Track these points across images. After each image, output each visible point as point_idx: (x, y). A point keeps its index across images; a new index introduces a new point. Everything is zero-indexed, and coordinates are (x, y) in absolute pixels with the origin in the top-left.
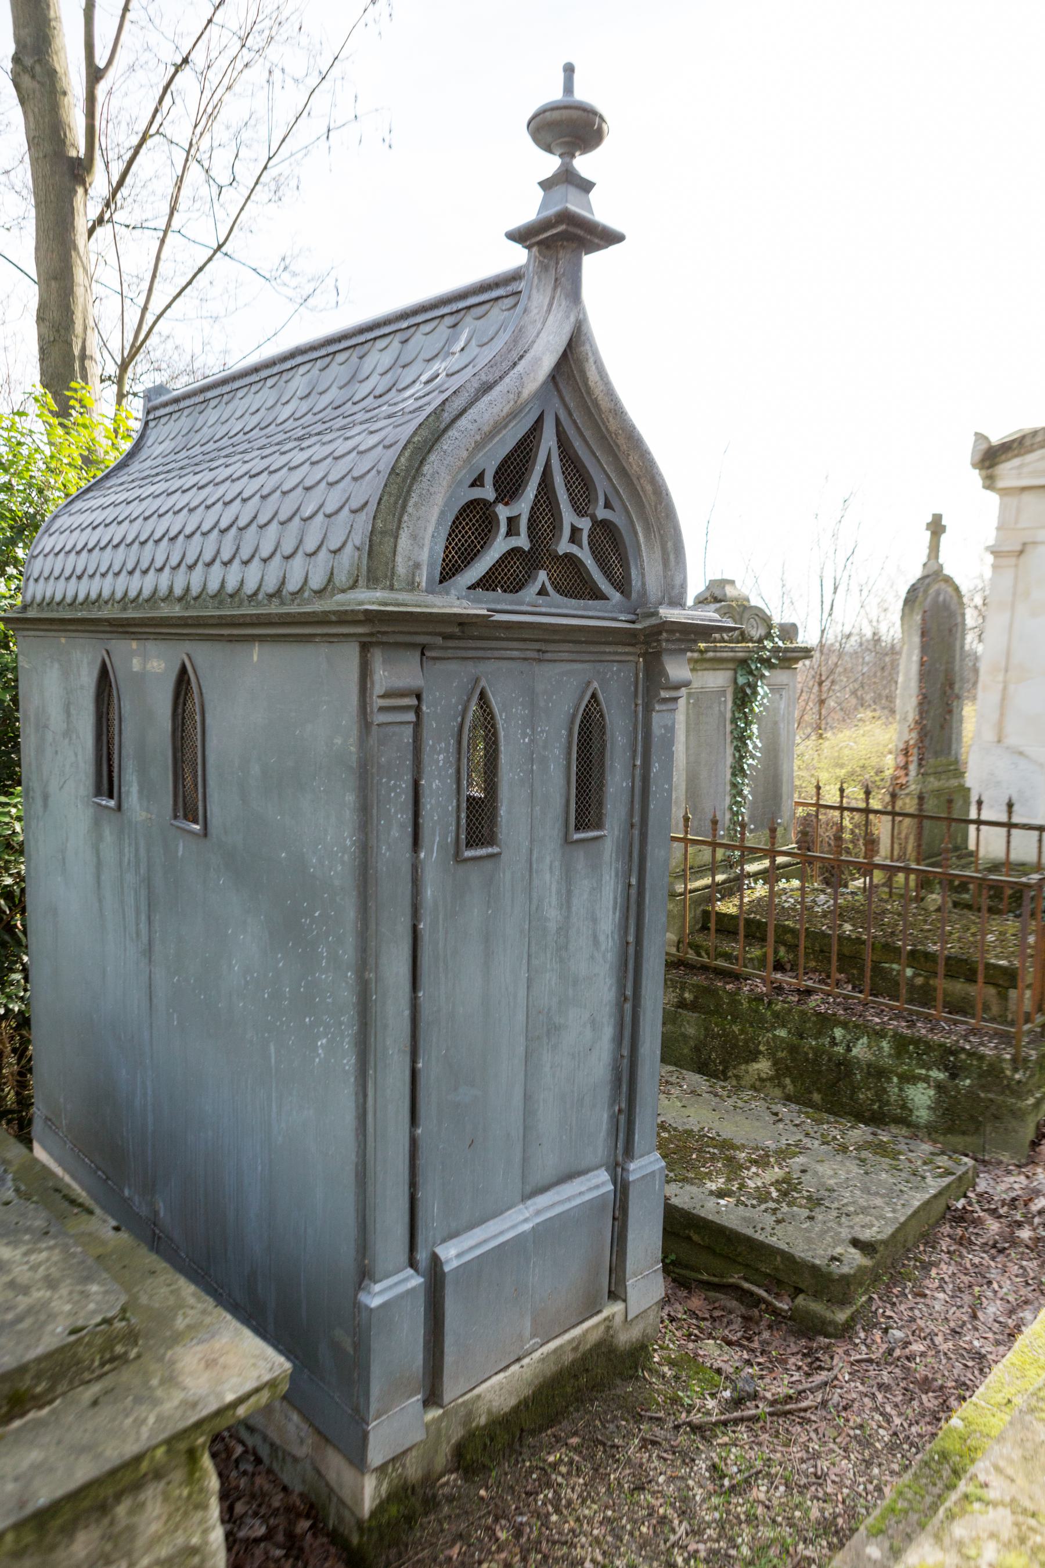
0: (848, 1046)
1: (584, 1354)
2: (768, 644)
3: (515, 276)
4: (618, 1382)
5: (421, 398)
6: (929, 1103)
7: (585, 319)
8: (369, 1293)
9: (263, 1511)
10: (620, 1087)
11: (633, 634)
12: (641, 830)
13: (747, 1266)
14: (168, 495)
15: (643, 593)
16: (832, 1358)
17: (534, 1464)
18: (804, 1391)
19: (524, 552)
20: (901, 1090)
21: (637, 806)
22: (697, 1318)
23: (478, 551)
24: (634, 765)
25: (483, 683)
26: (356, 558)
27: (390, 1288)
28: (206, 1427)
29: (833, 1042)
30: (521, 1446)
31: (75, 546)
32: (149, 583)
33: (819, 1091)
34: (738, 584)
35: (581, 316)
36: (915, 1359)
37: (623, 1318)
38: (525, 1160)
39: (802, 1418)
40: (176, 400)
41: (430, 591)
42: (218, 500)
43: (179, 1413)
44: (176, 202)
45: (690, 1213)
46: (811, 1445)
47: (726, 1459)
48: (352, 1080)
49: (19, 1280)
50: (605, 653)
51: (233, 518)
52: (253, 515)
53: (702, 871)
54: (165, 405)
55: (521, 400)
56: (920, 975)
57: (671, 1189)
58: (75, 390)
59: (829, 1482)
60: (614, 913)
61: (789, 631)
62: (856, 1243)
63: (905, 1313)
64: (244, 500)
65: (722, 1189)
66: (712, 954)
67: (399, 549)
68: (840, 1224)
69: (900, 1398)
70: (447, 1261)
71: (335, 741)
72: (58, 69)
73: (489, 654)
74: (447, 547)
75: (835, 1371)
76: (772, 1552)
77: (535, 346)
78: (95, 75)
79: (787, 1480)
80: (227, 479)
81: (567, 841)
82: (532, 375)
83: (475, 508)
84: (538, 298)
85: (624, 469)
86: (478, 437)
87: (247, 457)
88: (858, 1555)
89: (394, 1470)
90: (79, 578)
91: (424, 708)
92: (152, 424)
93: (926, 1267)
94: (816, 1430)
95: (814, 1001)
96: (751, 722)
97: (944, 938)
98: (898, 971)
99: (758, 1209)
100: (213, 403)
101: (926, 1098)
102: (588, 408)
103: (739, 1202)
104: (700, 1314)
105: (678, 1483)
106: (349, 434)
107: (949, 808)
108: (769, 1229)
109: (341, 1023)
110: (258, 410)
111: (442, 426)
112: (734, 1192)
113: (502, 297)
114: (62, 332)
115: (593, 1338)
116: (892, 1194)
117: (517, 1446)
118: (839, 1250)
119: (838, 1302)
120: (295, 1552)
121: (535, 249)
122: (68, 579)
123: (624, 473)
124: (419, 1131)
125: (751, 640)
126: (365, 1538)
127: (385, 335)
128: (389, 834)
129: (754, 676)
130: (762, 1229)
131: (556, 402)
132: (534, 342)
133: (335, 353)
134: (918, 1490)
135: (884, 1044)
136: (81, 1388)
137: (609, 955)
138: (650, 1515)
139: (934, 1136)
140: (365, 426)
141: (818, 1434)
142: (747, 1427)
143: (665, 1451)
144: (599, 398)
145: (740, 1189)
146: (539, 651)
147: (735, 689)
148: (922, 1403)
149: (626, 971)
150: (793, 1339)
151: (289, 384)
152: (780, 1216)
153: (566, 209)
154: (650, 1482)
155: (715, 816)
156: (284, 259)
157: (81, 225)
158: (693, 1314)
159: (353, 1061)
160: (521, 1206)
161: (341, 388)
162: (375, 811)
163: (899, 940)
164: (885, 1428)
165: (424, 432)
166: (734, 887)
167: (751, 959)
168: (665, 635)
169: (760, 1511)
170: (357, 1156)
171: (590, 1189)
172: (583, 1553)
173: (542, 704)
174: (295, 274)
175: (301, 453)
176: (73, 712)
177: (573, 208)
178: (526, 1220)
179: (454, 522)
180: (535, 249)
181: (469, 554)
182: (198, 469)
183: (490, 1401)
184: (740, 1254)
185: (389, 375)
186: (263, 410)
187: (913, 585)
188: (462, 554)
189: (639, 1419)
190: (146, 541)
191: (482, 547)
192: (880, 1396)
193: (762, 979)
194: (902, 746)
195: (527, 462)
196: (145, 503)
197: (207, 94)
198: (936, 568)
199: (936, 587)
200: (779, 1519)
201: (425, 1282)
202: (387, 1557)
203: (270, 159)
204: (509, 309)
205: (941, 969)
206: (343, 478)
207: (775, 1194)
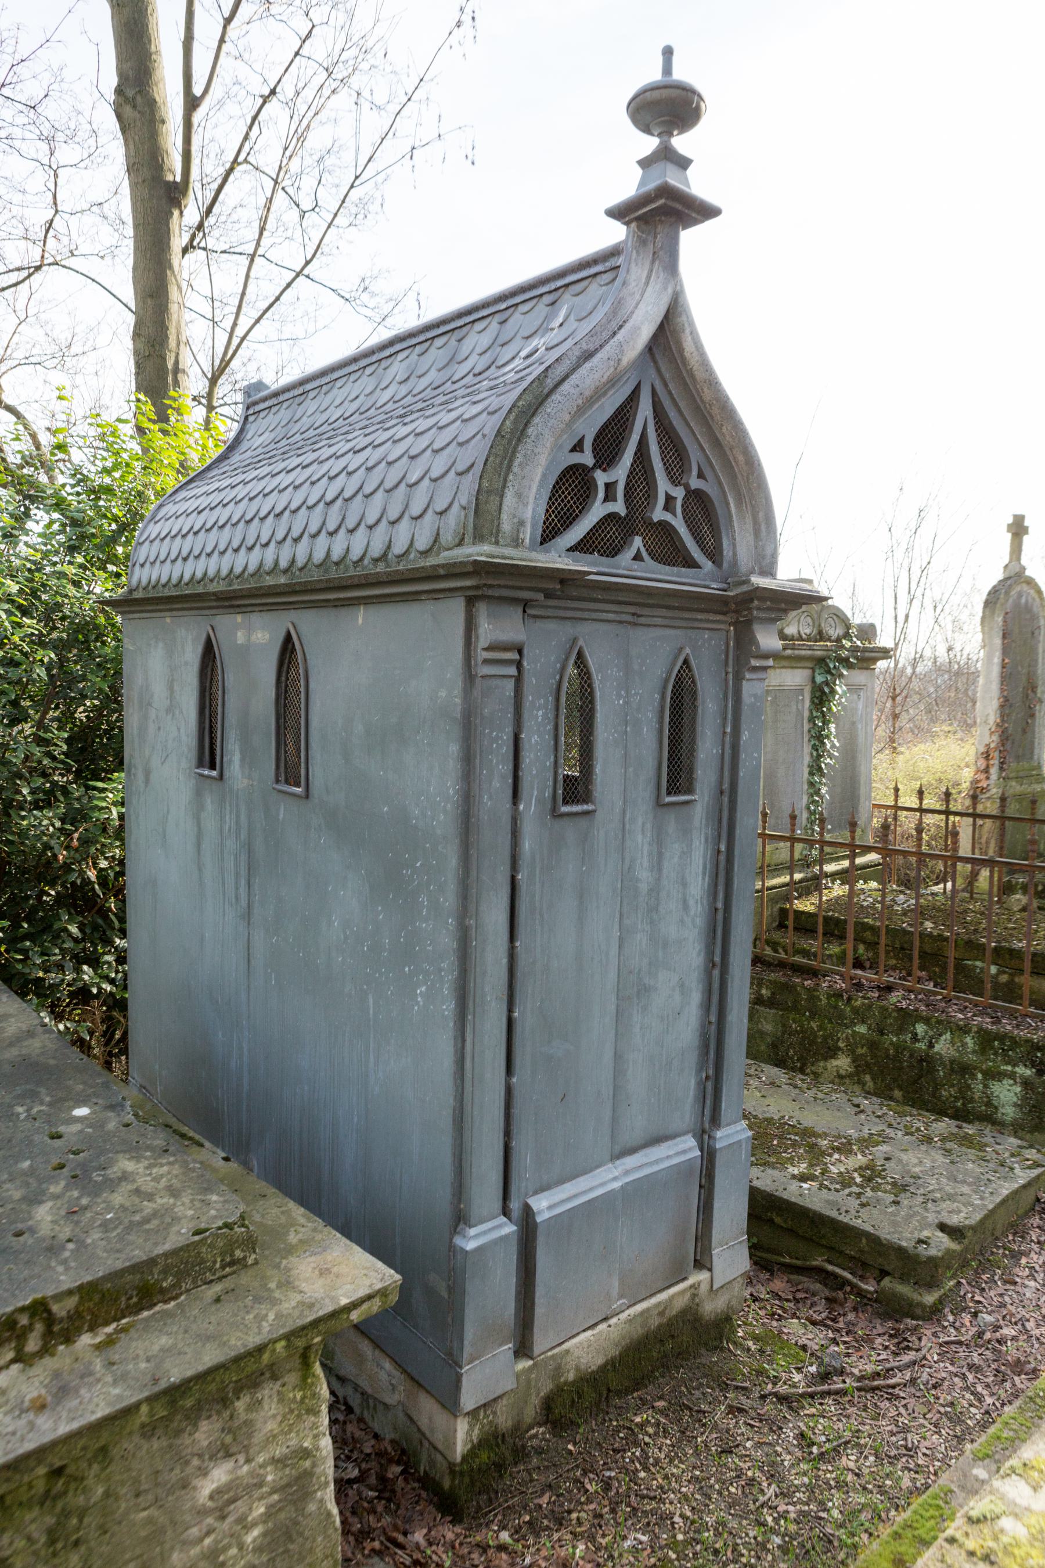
0: (930, 1042)
1: (670, 1320)
2: (847, 644)
3: (615, 252)
4: (703, 1351)
5: (521, 371)
6: (1015, 1099)
7: (682, 291)
8: (464, 1236)
9: (355, 1456)
10: (707, 1053)
11: (724, 601)
12: (730, 796)
13: (831, 1248)
14: (273, 476)
15: (735, 563)
16: (920, 1339)
17: (621, 1423)
18: (892, 1369)
19: (620, 518)
20: (986, 1086)
21: (726, 773)
22: (780, 1298)
23: (577, 516)
24: (724, 733)
25: (581, 642)
26: (462, 517)
27: (485, 1233)
28: (322, 1327)
29: (915, 1038)
30: (608, 1406)
31: (180, 530)
32: (254, 560)
33: (900, 1088)
34: (816, 583)
35: (678, 288)
36: (1006, 1342)
37: (708, 1287)
38: (615, 1119)
39: (890, 1394)
40: (276, 394)
41: (531, 548)
42: (323, 476)
43: (296, 1313)
44: (265, 223)
45: (772, 1195)
46: (900, 1420)
47: (813, 1429)
48: (452, 1024)
49: (143, 1189)
50: (697, 620)
51: (339, 490)
52: (358, 486)
53: (779, 869)
54: (264, 399)
55: (620, 368)
56: (1004, 972)
57: (755, 1172)
58: (175, 399)
59: (920, 1454)
60: (703, 879)
61: (868, 631)
62: (943, 1227)
63: (995, 1299)
64: (349, 474)
65: (804, 1174)
66: (790, 950)
67: (505, 507)
68: (926, 1210)
69: (992, 1378)
70: (539, 1212)
71: (440, 694)
72: (158, 99)
73: (586, 615)
74: (547, 511)
75: (924, 1351)
76: (863, 1517)
77: (634, 316)
78: (192, 103)
79: (877, 1451)
80: (331, 457)
81: (659, 804)
82: (631, 343)
83: (574, 473)
84: (636, 272)
85: (717, 439)
86: (580, 402)
87: (350, 436)
88: (965, 1476)
89: (486, 1416)
90: (185, 559)
91: (525, 664)
92: (251, 419)
93: (1016, 1256)
94: (905, 1406)
95: (894, 997)
96: (829, 721)
97: (1029, 936)
98: (982, 969)
99: (842, 1193)
100: (312, 394)
101: (1012, 1094)
102: (683, 378)
103: (821, 1186)
104: (783, 1295)
105: (766, 1449)
106: (451, 407)
107: (1033, 809)
108: (853, 1212)
109: (440, 970)
110: (357, 397)
111: (546, 391)
112: (817, 1177)
113: (601, 273)
114: (157, 347)
115: (680, 1304)
116: (977, 1184)
117: (604, 1406)
118: (926, 1233)
119: (925, 1285)
120: (387, 1495)
121: (633, 225)
122: (174, 561)
123: (717, 443)
124: (514, 1080)
125: (829, 640)
126: (457, 1482)
127: (483, 318)
128: (491, 783)
129: (832, 675)
130: (847, 1212)
131: (652, 373)
132: (632, 313)
133: (433, 338)
134: (1024, 1422)
135: (969, 1040)
136: (203, 1287)
137: (698, 921)
138: (738, 1476)
139: (1020, 1134)
140: (466, 399)
141: (907, 1409)
142: (834, 1400)
143: (752, 1419)
144: (695, 368)
145: (823, 1174)
146: (634, 614)
147: (813, 688)
148: (1014, 1385)
149: (714, 938)
150: (879, 1321)
151: (388, 371)
152: (864, 1200)
153: (666, 183)
154: (737, 1446)
155: (793, 811)
156: (363, 280)
157: (179, 240)
158: (776, 1295)
159: (453, 1006)
160: (610, 1165)
161: (439, 370)
162: (477, 761)
163: (984, 937)
164: (976, 1407)
165: (528, 397)
166: (813, 885)
167: (830, 956)
168: (756, 602)
169: (850, 1477)
170: (455, 1100)
171: (678, 1154)
172: (672, 1509)
173: (636, 667)
174: (374, 295)
175: (405, 428)
176: (176, 688)
177: (673, 182)
178: (615, 1179)
179: (554, 487)
180: (633, 225)
181: (568, 518)
182: (300, 452)
183: (579, 1358)
184: (823, 1237)
185: (488, 354)
186: (362, 397)
187: (994, 587)
188: (562, 517)
189: (724, 1387)
190: (252, 520)
191: (580, 512)
192: (970, 1377)
193: (841, 975)
194: (982, 749)
195: (624, 431)
196: (249, 486)
197: (296, 118)
198: (1017, 570)
199: (1018, 588)
200: (870, 1487)
201: (518, 1231)
202: (478, 1502)
203: (357, 177)
204: (607, 284)
205: (1027, 965)
206: (448, 445)
207: (858, 1180)
